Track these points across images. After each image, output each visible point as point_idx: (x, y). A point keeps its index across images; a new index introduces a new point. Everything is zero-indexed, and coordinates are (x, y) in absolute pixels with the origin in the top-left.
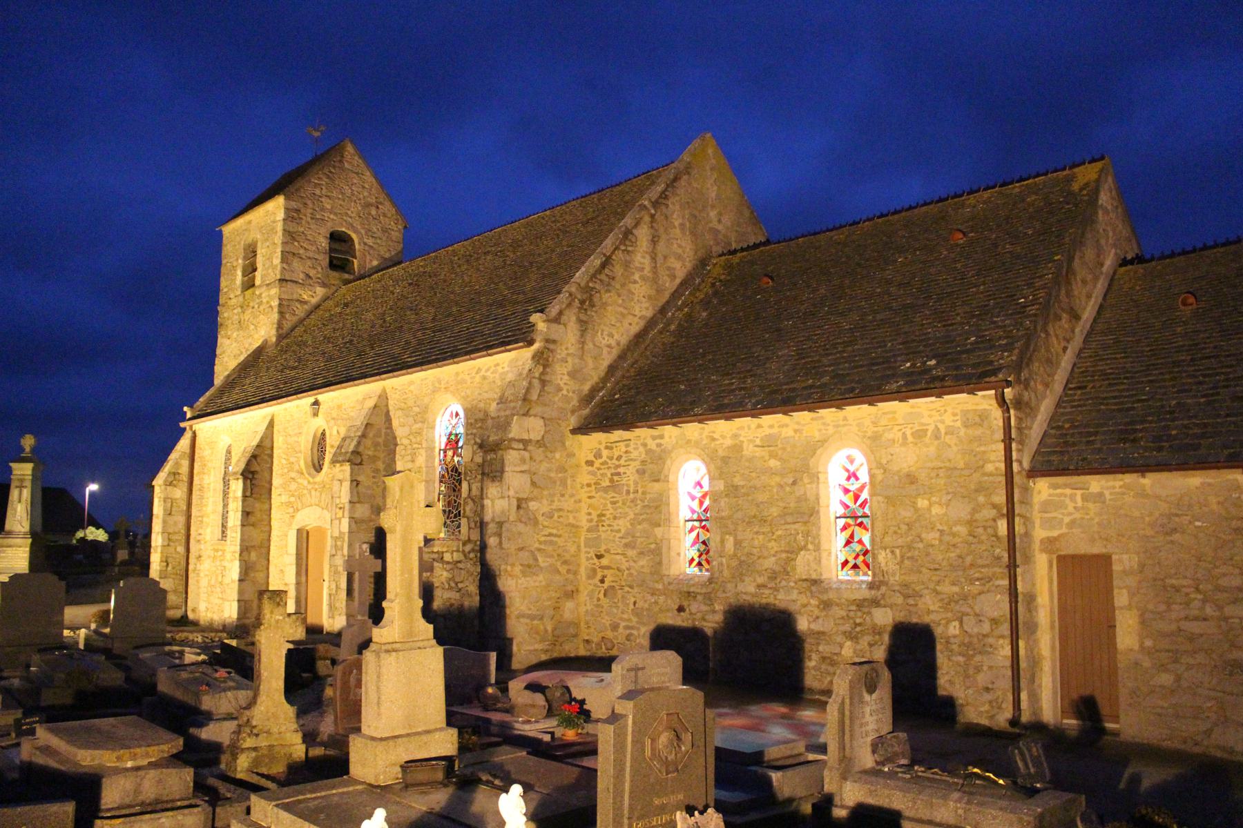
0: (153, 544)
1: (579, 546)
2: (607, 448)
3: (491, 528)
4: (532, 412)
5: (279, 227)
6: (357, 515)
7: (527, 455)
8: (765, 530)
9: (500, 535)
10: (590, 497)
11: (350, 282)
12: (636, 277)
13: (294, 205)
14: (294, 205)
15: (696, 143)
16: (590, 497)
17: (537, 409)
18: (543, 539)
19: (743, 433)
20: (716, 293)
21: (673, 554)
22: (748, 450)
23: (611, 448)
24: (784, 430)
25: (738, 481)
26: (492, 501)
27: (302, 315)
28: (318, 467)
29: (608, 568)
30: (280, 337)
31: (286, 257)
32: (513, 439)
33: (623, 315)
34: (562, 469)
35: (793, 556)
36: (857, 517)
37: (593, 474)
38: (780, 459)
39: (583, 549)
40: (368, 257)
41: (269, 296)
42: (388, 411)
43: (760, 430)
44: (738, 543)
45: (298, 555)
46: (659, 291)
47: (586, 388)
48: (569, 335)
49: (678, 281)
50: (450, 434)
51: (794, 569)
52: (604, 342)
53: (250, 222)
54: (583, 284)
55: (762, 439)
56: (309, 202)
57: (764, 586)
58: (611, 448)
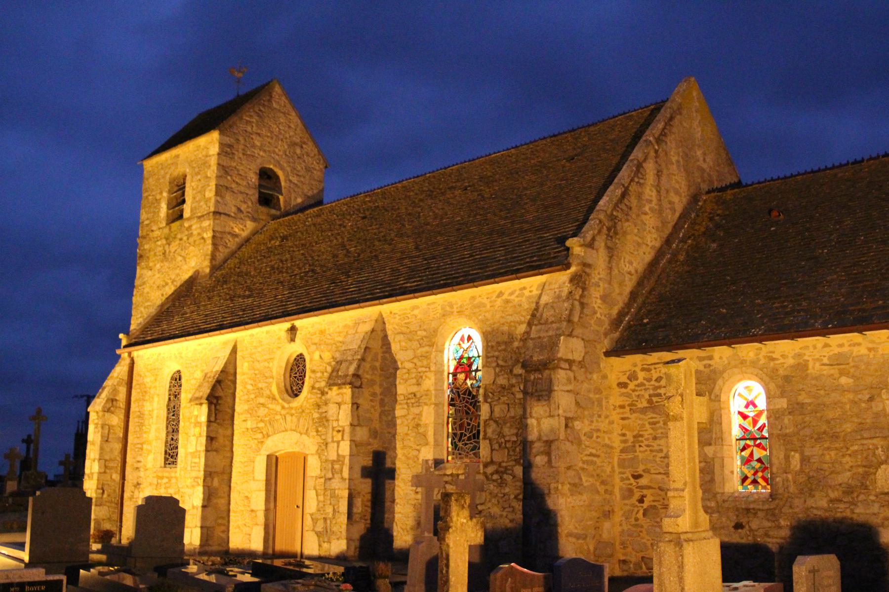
0: (87, 471)
1: (613, 467)
2: (643, 370)
3: (538, 446)
4: (575, 333)
5: (213, 161)
6: (358, 438)
7: (571, 374)
8: (837, 445)
9: (548, 454)
10: (623, 419)
11: (279, 218)
12: (647, 209)
13: (227, 140)
14: (227, 140)
15: (683, 86)
16: (623, 419)
17: (578, 331)
18: (585, 458)
19: (807, 352)
20: (718, 226)
21: (726, 472)
22: (814, 368)
23: (649, 370)
24: (855, 349)
25: (803, 398)
26: (538, 420)
27: (234, 247)
28: (294, 392)
29: (649, 487)
30: (214, 268)
31: (220, 190)
32: (561, 359)
33: (639, 244)
34: (598, 391)
35: (872, 470)
36: (755, 439)
37: (628, 395)
38: (853, 377)
39: (617, 470)
40: (293, 195)
41: (205, 229)
42: (386, 336)
43: (827, 349)
44: (804, 460)
45: (268, 481)
46: (664, 223)
47: (615, 312)
48: (599, 258)
49: (677, 215)
50: (462, 357)
51: (875, 482)
52: (626, 269)
53: (177, 156)
54: (609, 212)
55: (830, 358)
56: (241, 138)
57: (839, 501)
58: (649, 370)
